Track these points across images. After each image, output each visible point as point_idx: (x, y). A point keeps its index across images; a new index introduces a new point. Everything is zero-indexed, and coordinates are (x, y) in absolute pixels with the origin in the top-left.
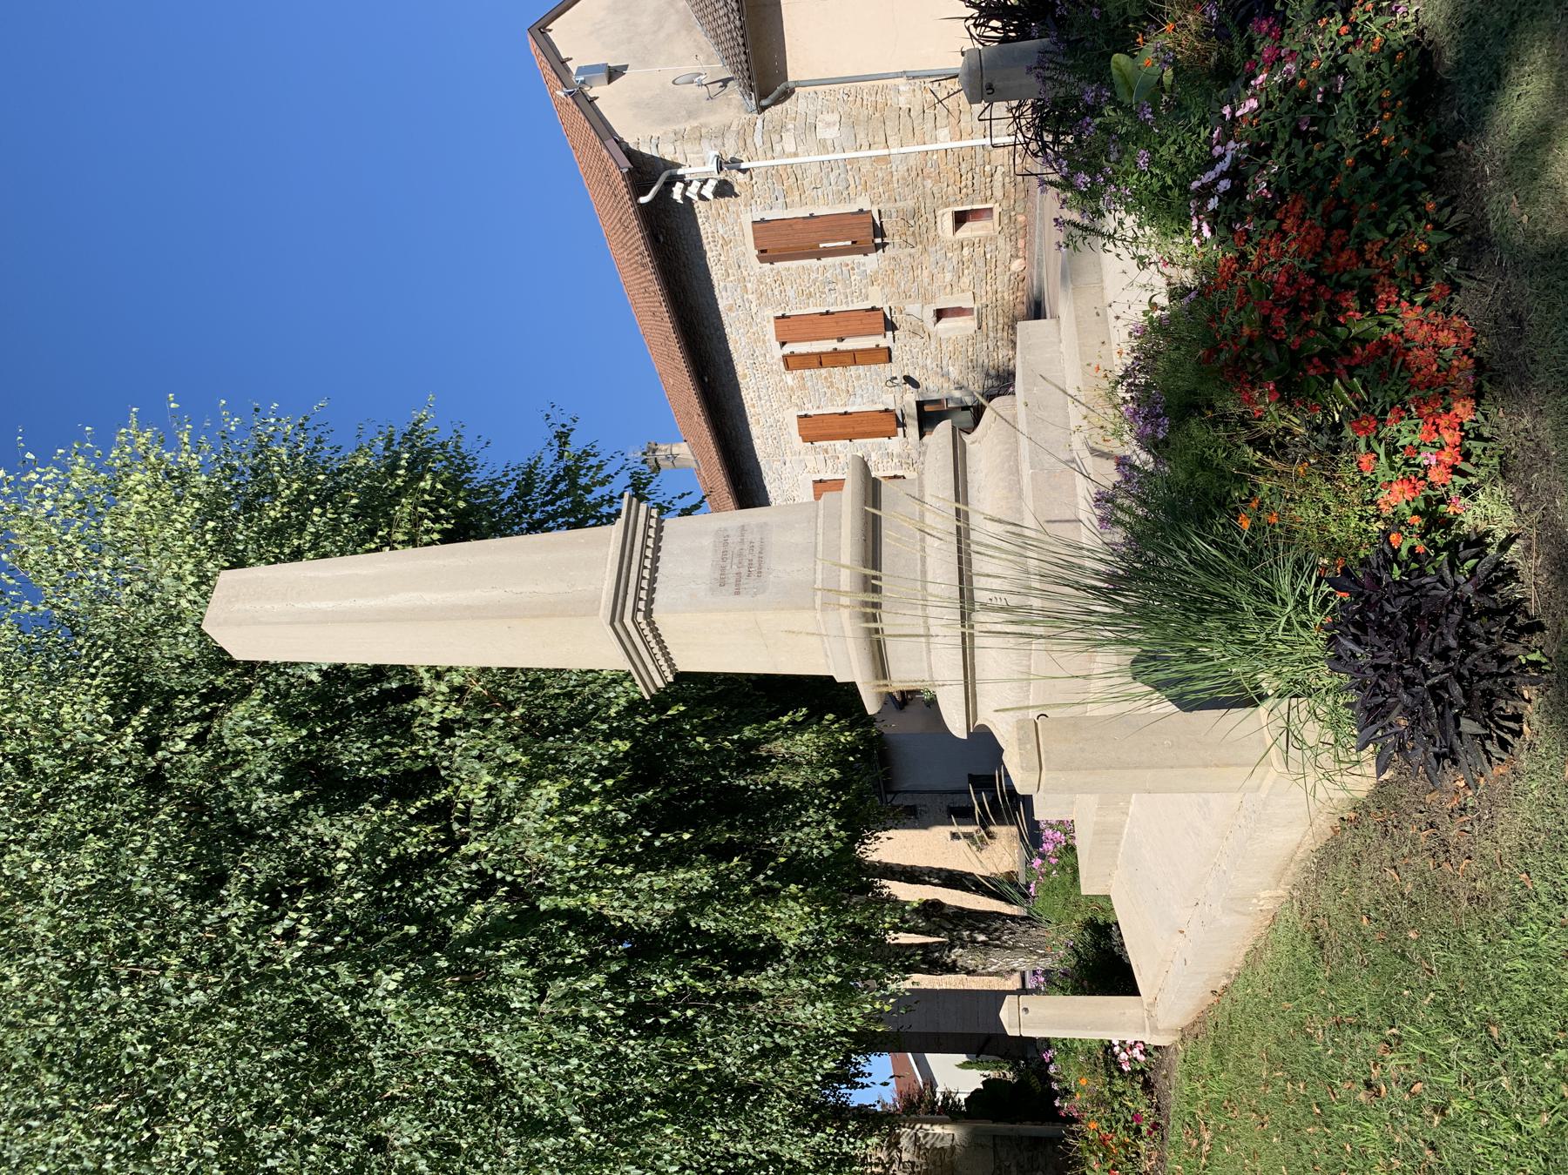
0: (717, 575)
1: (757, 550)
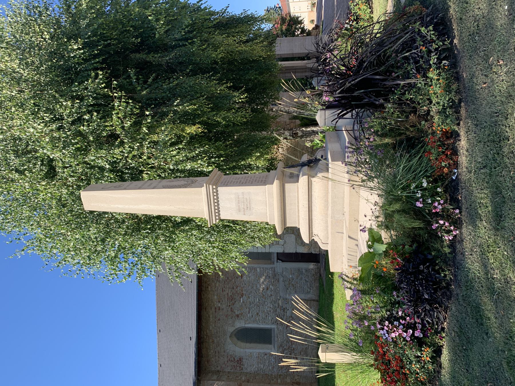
1: (248, 201)
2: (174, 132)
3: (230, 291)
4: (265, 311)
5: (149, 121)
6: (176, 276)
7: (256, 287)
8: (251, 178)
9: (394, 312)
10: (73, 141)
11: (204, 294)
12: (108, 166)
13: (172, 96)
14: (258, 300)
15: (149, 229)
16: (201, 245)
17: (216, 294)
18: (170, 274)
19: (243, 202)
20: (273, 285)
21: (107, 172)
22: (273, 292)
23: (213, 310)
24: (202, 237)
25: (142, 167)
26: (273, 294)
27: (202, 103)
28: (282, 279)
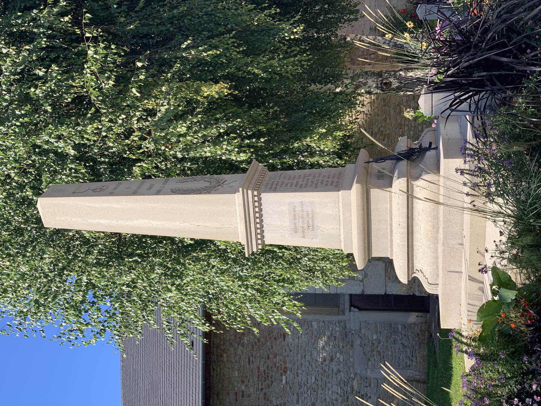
0: (293, 226)
1: (310, 216)
2: (183, 95)
3: (262, 363)
4: (328, 399)
5: (142, 77)
6: (182, 334)
7: (311, 355)
8: (314, 177)
9: (526, 385)
10: (17, 112)
11: (215, 367)
12: (72, 152)
13: (176, 30)
14: (313, 380)
15: (140, 256)
16: (224, 282)
17: (236, 367)
18: (169, 330)
19: (302, 217)
20: (341, 353)
21: (72, 162)
22: (341, 365)
23: (232, 396)
24: (225, 270)
25: (128, 152)
26: (342, 370)
27: (228, 44)
28: (358, 341)
